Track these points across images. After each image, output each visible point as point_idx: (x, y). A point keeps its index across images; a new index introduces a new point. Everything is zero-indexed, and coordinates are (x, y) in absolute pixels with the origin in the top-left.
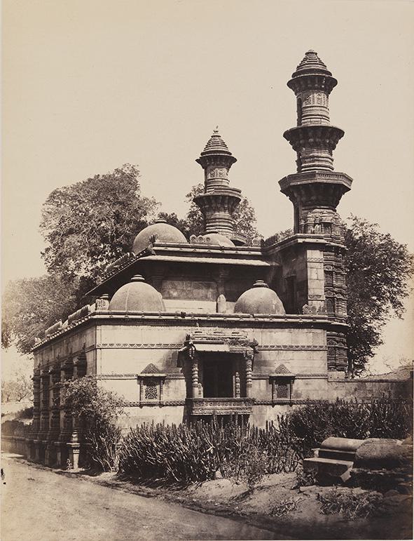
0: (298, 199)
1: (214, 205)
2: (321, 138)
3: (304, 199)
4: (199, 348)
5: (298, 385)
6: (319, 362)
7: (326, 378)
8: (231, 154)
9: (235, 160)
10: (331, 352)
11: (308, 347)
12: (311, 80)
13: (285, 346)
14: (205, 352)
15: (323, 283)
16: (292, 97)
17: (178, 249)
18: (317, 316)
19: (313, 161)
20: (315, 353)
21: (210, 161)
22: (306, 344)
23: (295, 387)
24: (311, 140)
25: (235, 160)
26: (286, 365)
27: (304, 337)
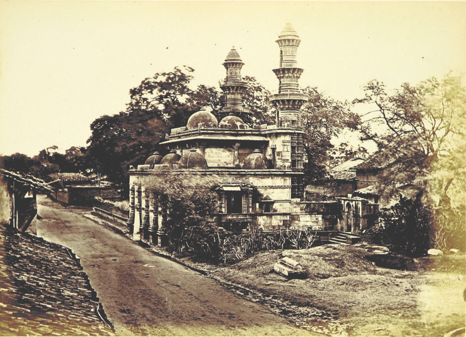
0: (279, 107)
1: (231, 92)
2: (292, 74)
3: (282, 107)
4: (225, 189)
5: (276, 206)
6: (286, 194)
7: (290, 202)
8: (241, 61)
9: (243, 64)
10: (293, 188)
11: (281, 186)
12: (287, 42)
13: (269, 186)
14: (228, 191)
15: (290, 153)
16: (277, 48)
17: (213, 132)
18: (286, 170)
19: (287, 86)
20: (285, 189)
21: (230, 65)
22: (280, 185)
23: (274, 207)
24: (287, 106)
25: (243, 64)
26: (269, 196)
27: (279, 181)
